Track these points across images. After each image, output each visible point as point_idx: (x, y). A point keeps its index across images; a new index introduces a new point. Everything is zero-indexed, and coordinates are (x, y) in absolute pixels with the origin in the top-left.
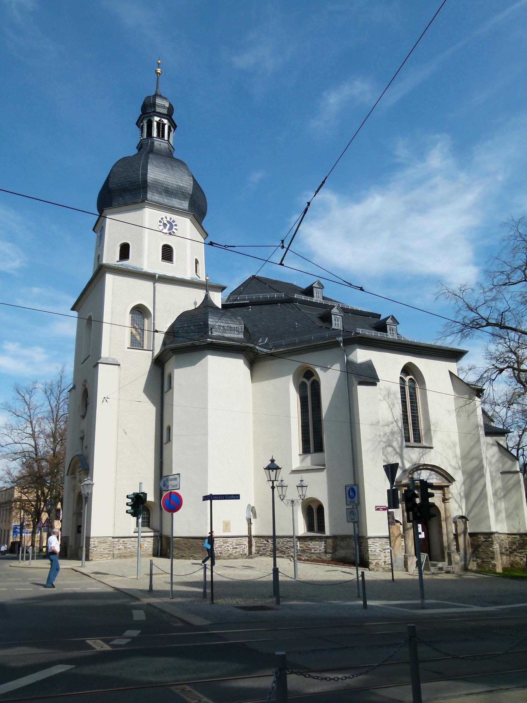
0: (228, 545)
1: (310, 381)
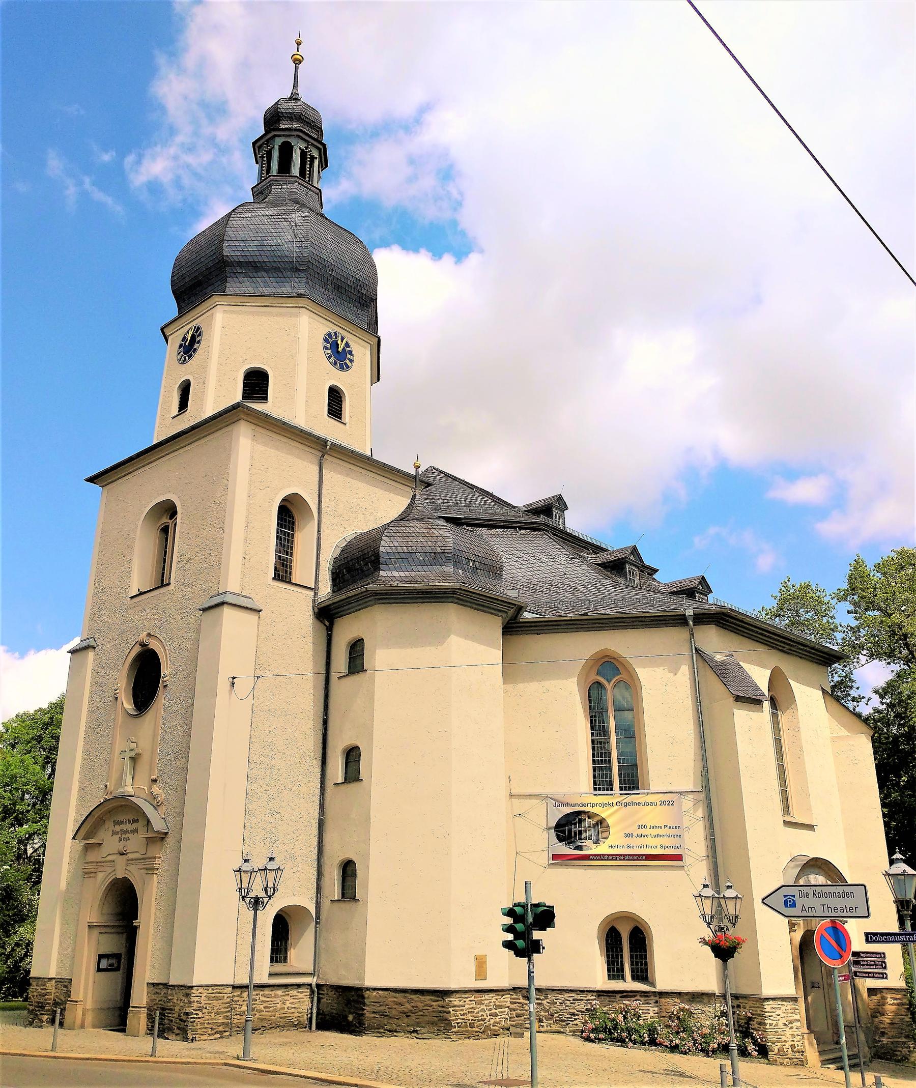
0: (482, 1007)
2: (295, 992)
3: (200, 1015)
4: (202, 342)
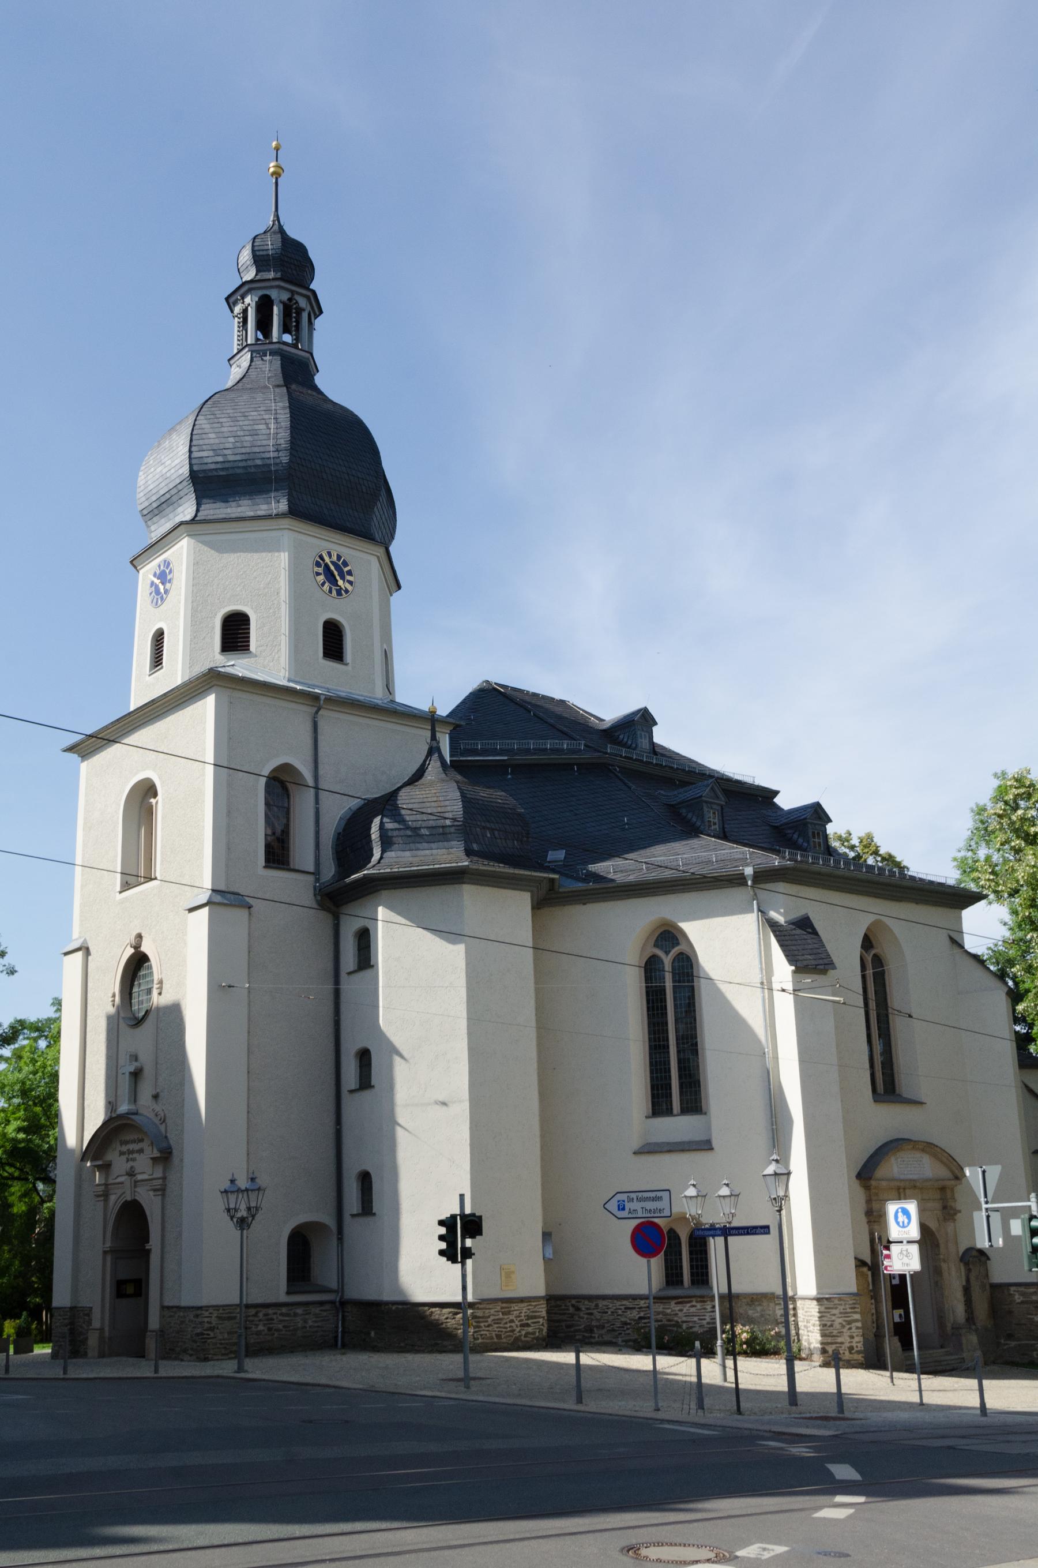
1: (671, 953)
2: (318, 1309)
3: (212, 1335)
4: (174, 582)
